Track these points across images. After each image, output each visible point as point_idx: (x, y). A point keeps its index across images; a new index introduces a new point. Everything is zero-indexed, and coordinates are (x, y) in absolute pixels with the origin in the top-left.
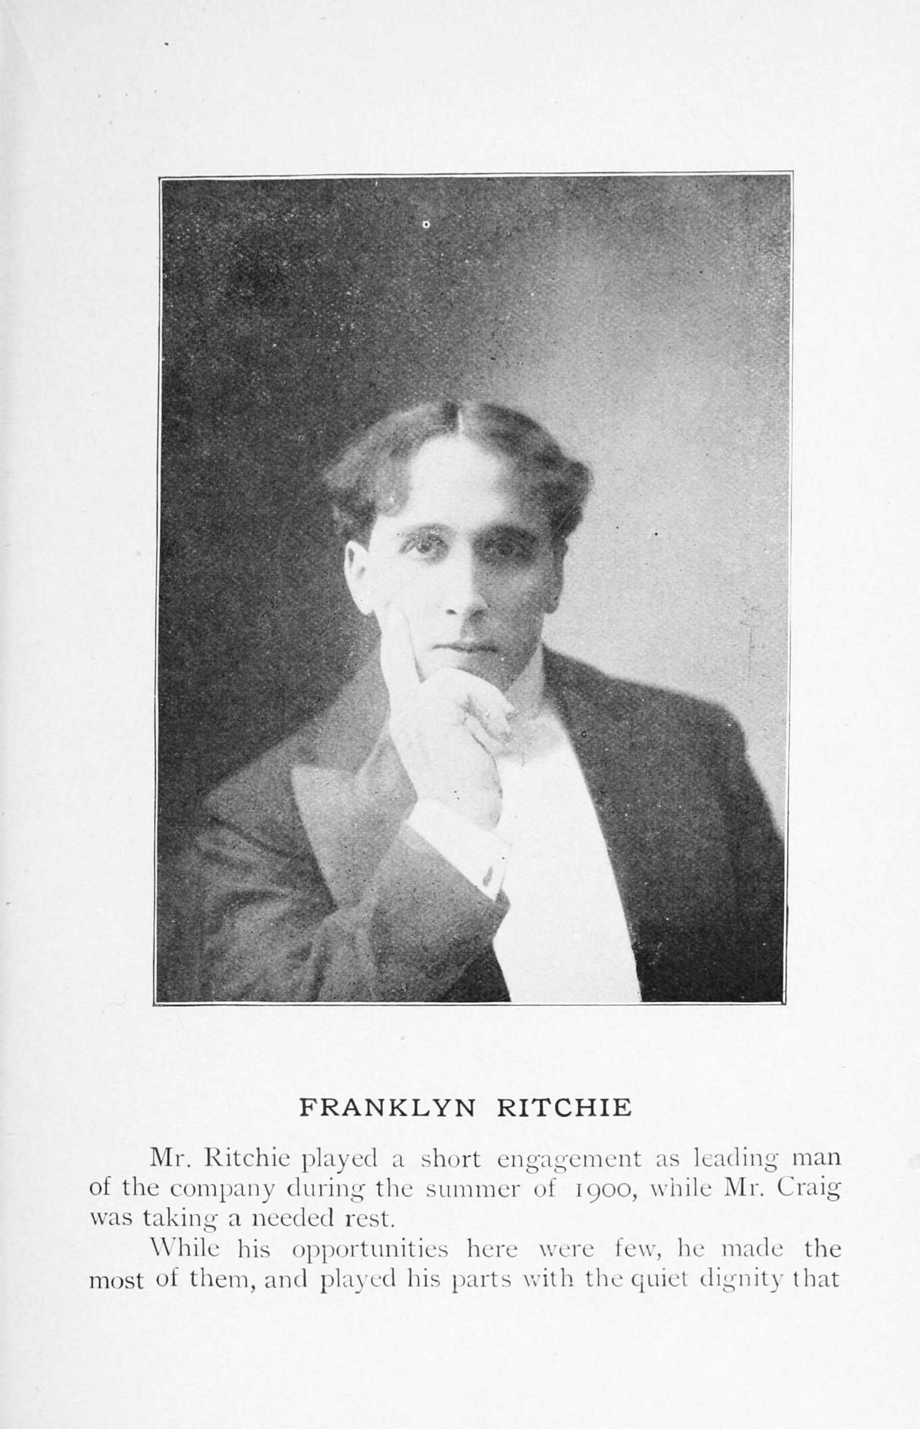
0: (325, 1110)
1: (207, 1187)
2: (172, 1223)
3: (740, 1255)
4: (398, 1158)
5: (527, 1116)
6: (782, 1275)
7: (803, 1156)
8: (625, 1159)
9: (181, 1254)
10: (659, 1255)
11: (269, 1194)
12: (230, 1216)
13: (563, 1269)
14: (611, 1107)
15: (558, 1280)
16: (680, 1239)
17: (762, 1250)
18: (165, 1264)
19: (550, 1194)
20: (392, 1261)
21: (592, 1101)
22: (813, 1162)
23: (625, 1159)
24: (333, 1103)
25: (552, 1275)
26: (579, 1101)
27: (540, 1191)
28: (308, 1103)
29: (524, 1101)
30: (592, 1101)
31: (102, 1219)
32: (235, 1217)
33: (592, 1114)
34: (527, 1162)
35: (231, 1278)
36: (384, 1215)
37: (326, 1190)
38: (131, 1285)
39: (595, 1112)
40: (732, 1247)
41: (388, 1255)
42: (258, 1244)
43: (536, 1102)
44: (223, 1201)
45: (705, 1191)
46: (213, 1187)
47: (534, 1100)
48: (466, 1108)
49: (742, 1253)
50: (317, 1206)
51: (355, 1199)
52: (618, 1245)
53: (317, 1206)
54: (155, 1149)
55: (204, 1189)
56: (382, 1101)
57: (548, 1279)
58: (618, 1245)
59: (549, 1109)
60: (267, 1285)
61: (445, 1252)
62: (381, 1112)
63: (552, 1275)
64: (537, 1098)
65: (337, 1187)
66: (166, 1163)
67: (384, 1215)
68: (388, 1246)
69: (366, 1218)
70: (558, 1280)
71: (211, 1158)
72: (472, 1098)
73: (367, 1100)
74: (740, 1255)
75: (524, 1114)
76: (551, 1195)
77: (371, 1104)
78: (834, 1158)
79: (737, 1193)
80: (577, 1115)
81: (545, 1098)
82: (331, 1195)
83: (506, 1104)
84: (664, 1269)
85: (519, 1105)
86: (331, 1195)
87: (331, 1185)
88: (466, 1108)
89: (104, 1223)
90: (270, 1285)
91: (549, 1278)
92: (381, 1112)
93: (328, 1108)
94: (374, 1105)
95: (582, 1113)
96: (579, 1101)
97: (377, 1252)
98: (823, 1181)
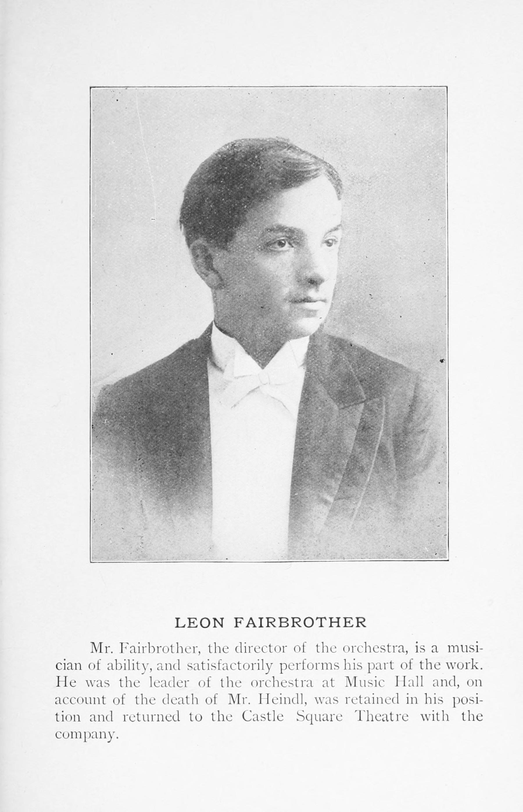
0: (190, 624)
1: (76, 733)
4: (435, 647)
9: (426, 703)
10: (151, 669)
11: (269, 669)
12: (91, 716)
13: (443, 711)
14: (342, 622)
15: (440, 717)
17: (172, 684)
19: (466, 668)
20: (178, 707)
21: (338, 618)
24: (273, 620)
25: (437, 714)
26: (331, 618)
27: (404, 666)
28: (239, 620)
30: (338, 618)
31: (93, 684)
33: (338, 626)
34: (192, 653)
37: (255, 667)
39: (340, 625)
41: (95, 703)
42: (410, 697)
46: (79, 733)
47: (317, 618)
48: (219, 622)
54: (93, 643)
55: (74, 734)
57: (267, 717)
60: (91, 720)
61: (107, 684)
63: (437, 714)
64: (319, 617)
66: (99, 651)
68: (412, 698)
69: (286, 682)
70: (440, 717)
72: (222, 617)
73: (214, 618)
76: (410, 669)
78: (78, 666)
80: (292, 627)
84: (433, 711)
85: (278, 621)
87: (259, 664)
88: (219, 622)
89: (94, 686)
90: (93, 720)
91: (435, 716)
93: (270, 623)
95: (332, 625)
96: (331, 618)
97: (146, 719)
98: (354, 661)
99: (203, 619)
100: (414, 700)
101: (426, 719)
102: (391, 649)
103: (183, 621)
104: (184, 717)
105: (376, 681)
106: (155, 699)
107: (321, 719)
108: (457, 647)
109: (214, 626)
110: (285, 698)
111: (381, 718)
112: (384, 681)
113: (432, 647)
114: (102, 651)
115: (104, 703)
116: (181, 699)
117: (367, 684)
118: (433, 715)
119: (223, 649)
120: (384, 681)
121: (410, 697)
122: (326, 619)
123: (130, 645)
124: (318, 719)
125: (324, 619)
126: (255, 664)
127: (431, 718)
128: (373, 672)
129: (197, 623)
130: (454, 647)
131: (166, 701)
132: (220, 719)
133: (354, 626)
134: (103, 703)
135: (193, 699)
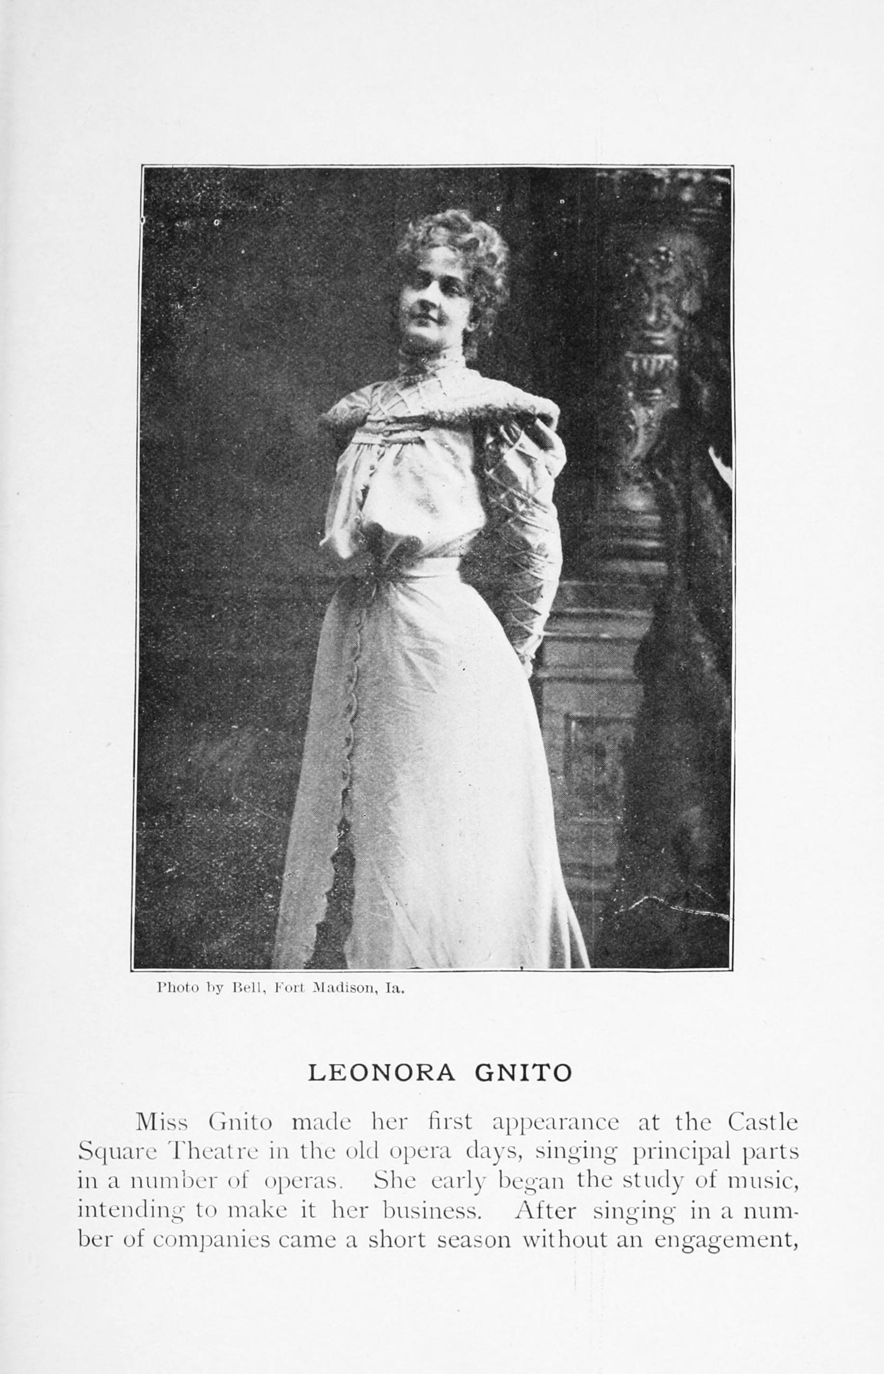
0: (420, 1076)
2: (267, 1214)
3: (245, 1216)
5: (527, 1080)
6: (682, 1177)
7: (302, 1121)
8: (776, 1241)
16: (334, 1201)
18: (534, 1228)
22: (312, 1127)
23: (776, 1241)
24: (428, 1068)
25: (551, 1236)
29: (525, 1066)
32: (114, 1180)
35: (670, 1238)
36: (636, 1176)
37: (656, 1153)
38: (374, 1244)
40: (238, 1209)
42: (695, 1205)
43: (536, 1067)
44: (701, 1163)
45: (792, 1125)
47: (535, 1065)
49: (248, 1214)
50: (759, 1168)
51: (608, 1161)
52: (540, 1208)
53: (759, 1168)
55: (185, 1240)
56: (513, 1066)
58: (540, 1208)
59: (548, 1073)
60: (619, 1245)
62: (512, 1077)
63: (551, 1236)
65: (110, 1150)
66: (151, 1128)
67: (636, 1176)
68: (87, 1207)
69: (522, 1181)
70: (556, 1241)
71: (433, 1121)
74: (245, 1216)
75: (525, 1079)
77: (503, 1070)
79: (148, 1128)
81: (546, 1063)
82: (661, 1157)
83: (424, 1068)
86: (661, 1157)
91: (548, 1239)
92: (512, 1077)
93: (423, 1073)
94: (382, 1072)
99: (354, 1067)
100: (704, 1212)
101: (531, 1244)
102: (235, 1153)
103: (323, 1070)
104: (431, 1241)
105: (778, 1178)
106: (285, 1209)
107: (122, 1156)
108: (694, 1121)
109: (373, 1077)
110: (87, 1207)
111: (459, 1242)
112: (791, 1179)
113: (641, 1121)
114: (155, 1128)
115: (313, 1215)
116: (219, 1151)
117: (763, 1183)
118: (544, 1237)
119: (702, 1123)
120: (791, 1179)
121: (696, 1206)
122: (549, 1068)
123: (746, 1117)
124: (115, 1154)
125: (547, 1067)
126: (451, 1118)
127: (540, 1242)
128: (643, 1161)
129: (346, 1072)
130: (302, 1121)
131: (472, 1152)
132: (502, 1245)
133: (326, 1079)
134: (102, 1215)
135: (335, 1209)
